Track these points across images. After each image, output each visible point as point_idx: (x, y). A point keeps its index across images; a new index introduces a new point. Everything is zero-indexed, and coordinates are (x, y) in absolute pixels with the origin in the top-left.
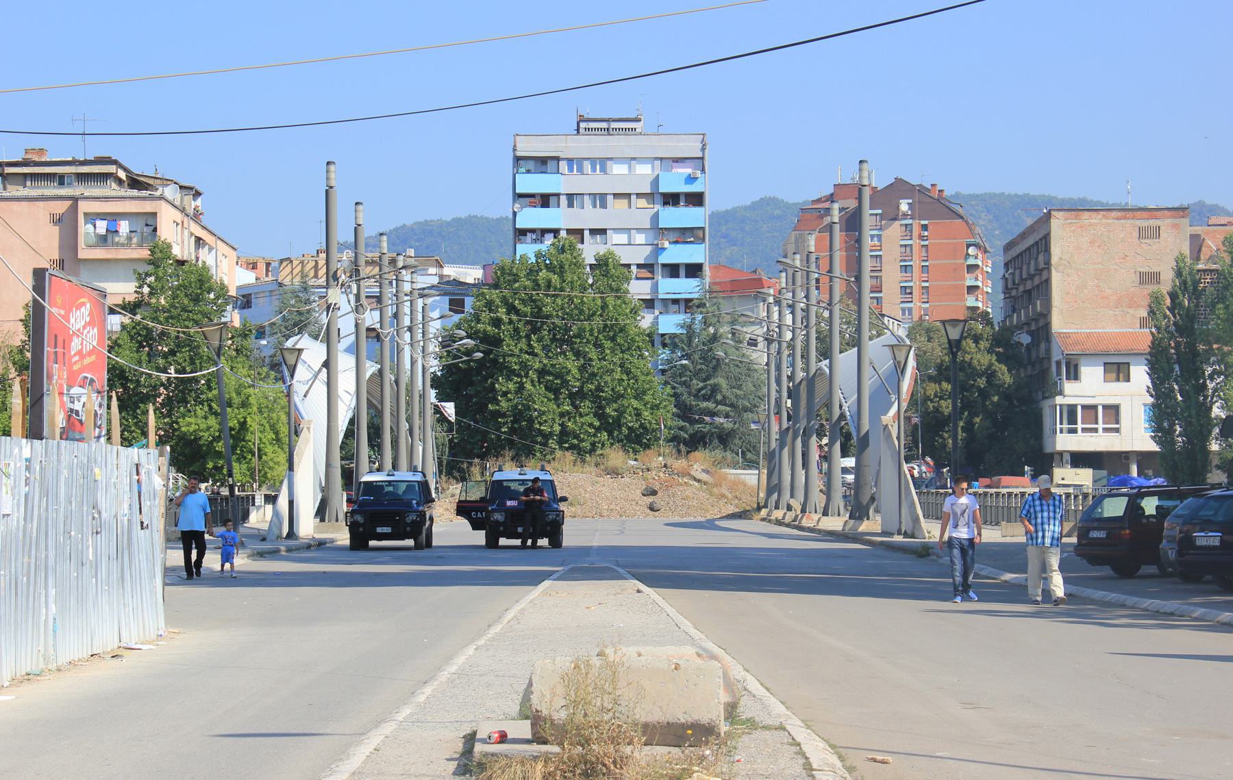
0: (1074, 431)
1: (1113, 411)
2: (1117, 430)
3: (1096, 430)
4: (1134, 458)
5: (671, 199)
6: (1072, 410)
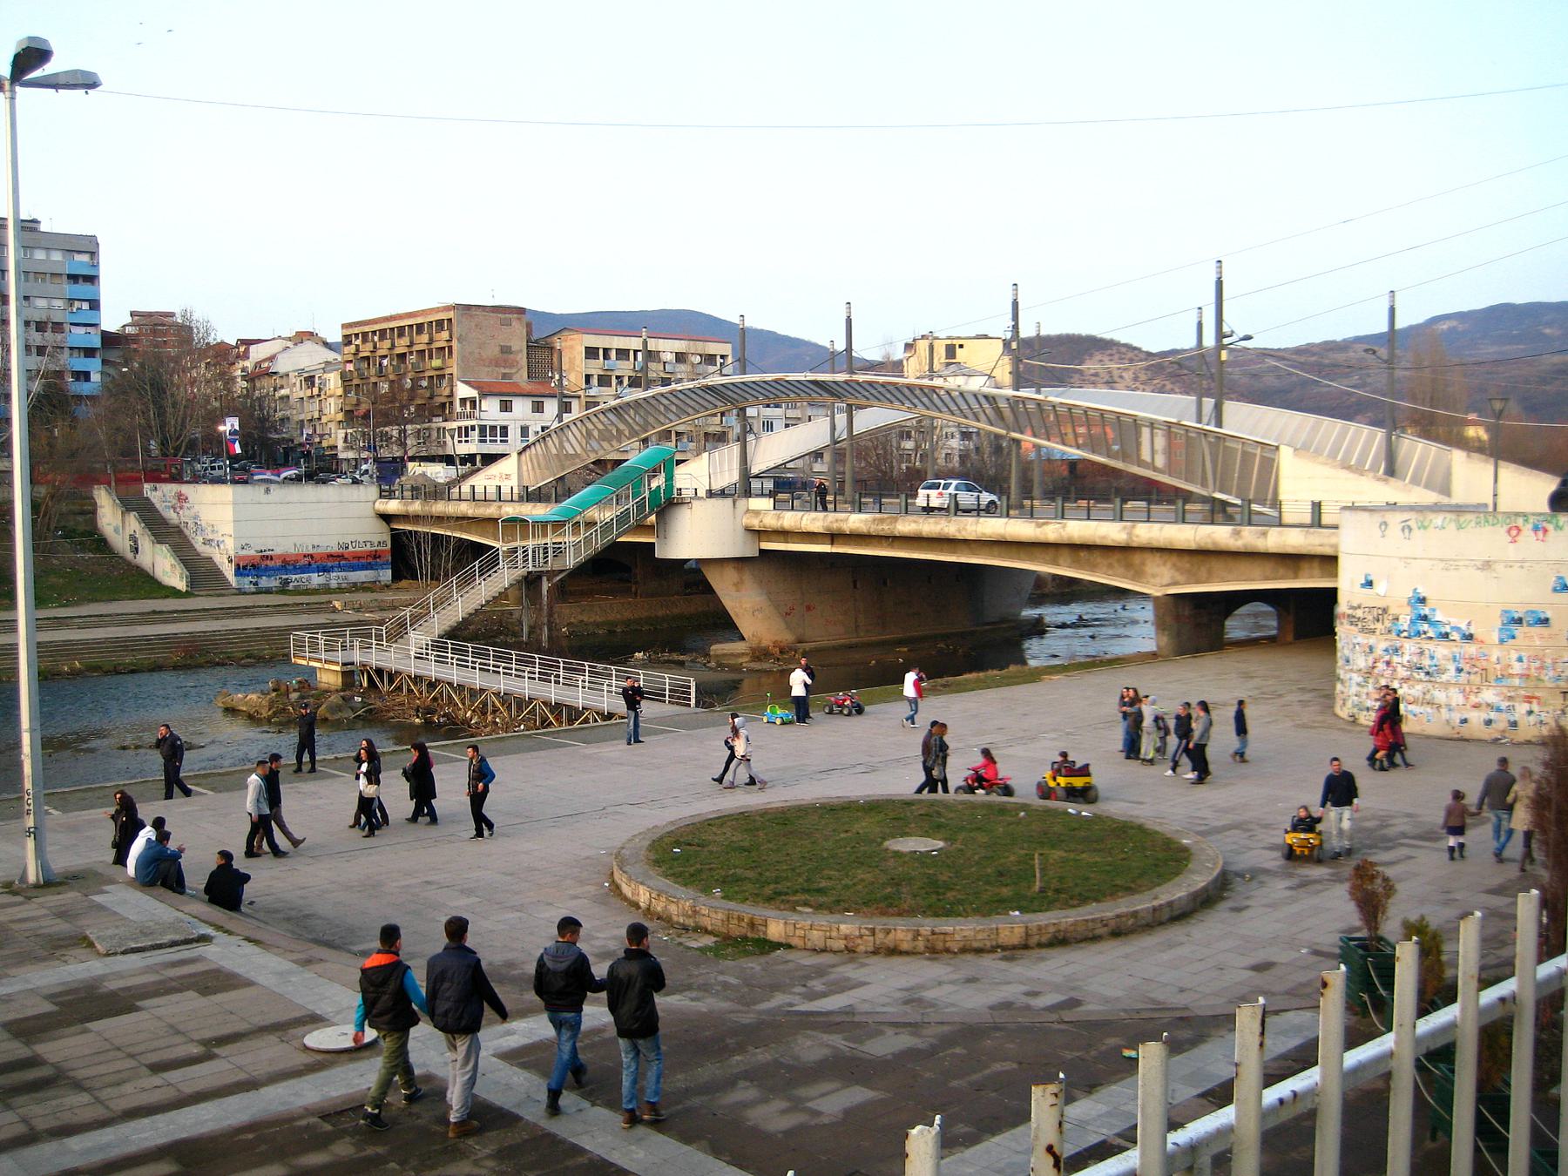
0: (485, 441)
2: (506, 441)
3: (496, 441)
5: (74, 278)
6: (483, 429)
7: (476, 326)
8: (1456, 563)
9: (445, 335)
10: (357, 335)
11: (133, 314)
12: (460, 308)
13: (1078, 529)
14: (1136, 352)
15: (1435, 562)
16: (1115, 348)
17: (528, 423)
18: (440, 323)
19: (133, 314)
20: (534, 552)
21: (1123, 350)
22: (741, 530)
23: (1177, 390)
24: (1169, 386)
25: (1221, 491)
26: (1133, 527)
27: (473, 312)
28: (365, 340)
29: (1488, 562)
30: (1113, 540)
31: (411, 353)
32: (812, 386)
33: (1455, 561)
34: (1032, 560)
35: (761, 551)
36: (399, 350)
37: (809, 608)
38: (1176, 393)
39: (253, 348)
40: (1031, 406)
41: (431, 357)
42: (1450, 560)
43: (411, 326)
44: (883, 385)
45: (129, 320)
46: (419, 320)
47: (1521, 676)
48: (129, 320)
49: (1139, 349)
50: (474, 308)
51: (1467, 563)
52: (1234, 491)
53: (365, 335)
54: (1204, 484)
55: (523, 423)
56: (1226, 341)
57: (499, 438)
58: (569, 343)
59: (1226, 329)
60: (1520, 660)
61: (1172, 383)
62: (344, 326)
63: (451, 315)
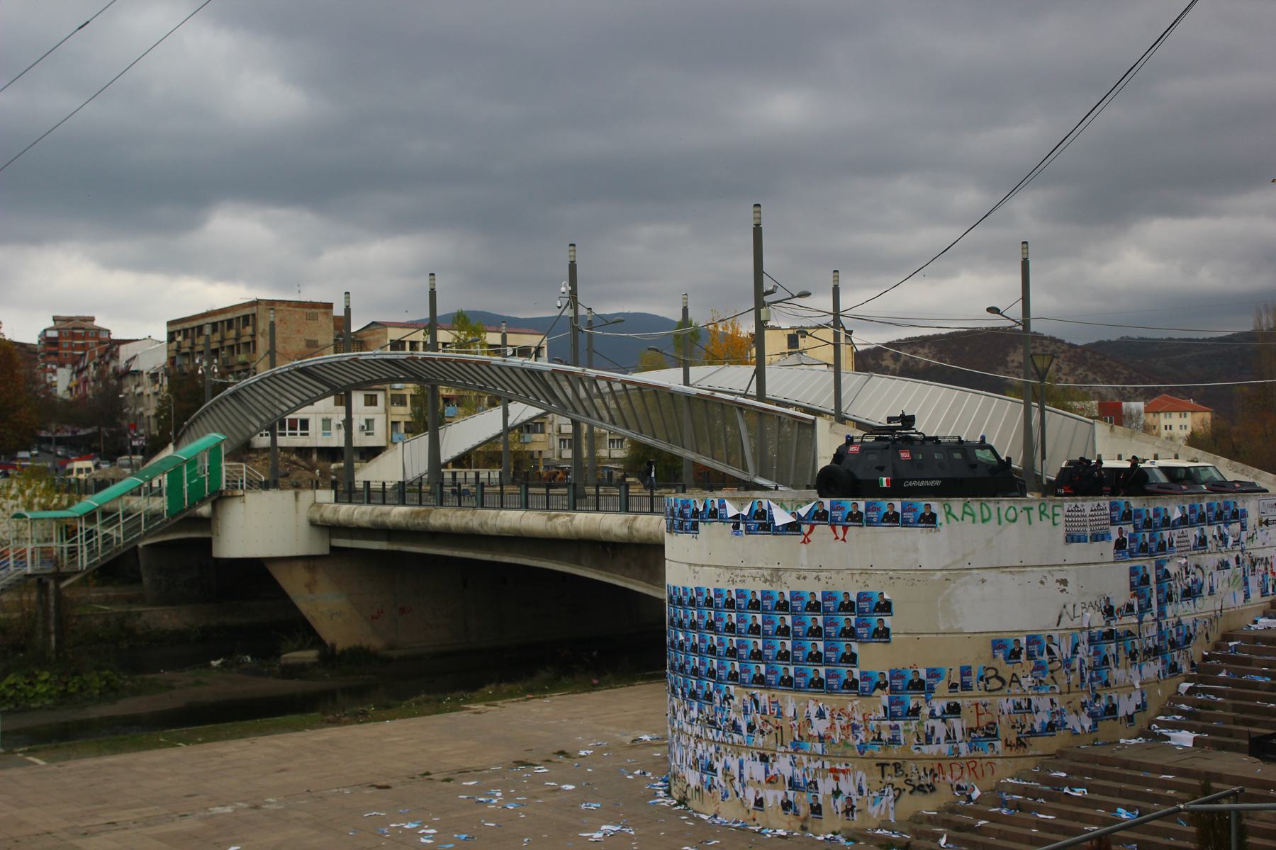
1: (305, 424)
2: (307, 434)
3: (296, 434)
4: (315, 451)
7: (281, 320)
8: (743, 573)
9: (249, 330)
10: (179, 332)
11: (55, 319)
12: (263, 303)
13: (584, 521)
14: (1059, 344)
15: (721, 571)
16: (1038, 341)
17: (329, 416)
18: (246, 318)
19: (55, 319)
20: (33, 553)
21: (1046, 342)
22: (304, 523)
23: (1099, 380)
24: (1091, 376)
25: (762, 476)
26: (635, 519)
27: (278, 307)
28: (185, 337)
29: (778, 570)
30: (615, 535)
31: (223, 349)
32: (386, 363)
33: (741, 569)
34: (577, 562)
35: (332, 548)
36: (214, 346)
37: (403, 611)
38: (1098, 383)
39: (123, 348)
40: (617, 387)
41: (239, 352)
42: (736, 568)
43: (222, 322)
44: (456, 362)
45: (51, 324)
46: (229, 316)
47: (821, 739)
48: (51, 324)
49: (1062, 342)
50: (277, 304)
51: (754, 572)
52: (774, 476)
53: (186, 331)
54: (745, 468)
55: (325, 416)
56: (767, 299)
57: (299, 431)
58: (377, 336)
59: (768, 286)
60: (821, 715)
61: (1094, 373)
62: (170, 324)
63: (254, 310)
